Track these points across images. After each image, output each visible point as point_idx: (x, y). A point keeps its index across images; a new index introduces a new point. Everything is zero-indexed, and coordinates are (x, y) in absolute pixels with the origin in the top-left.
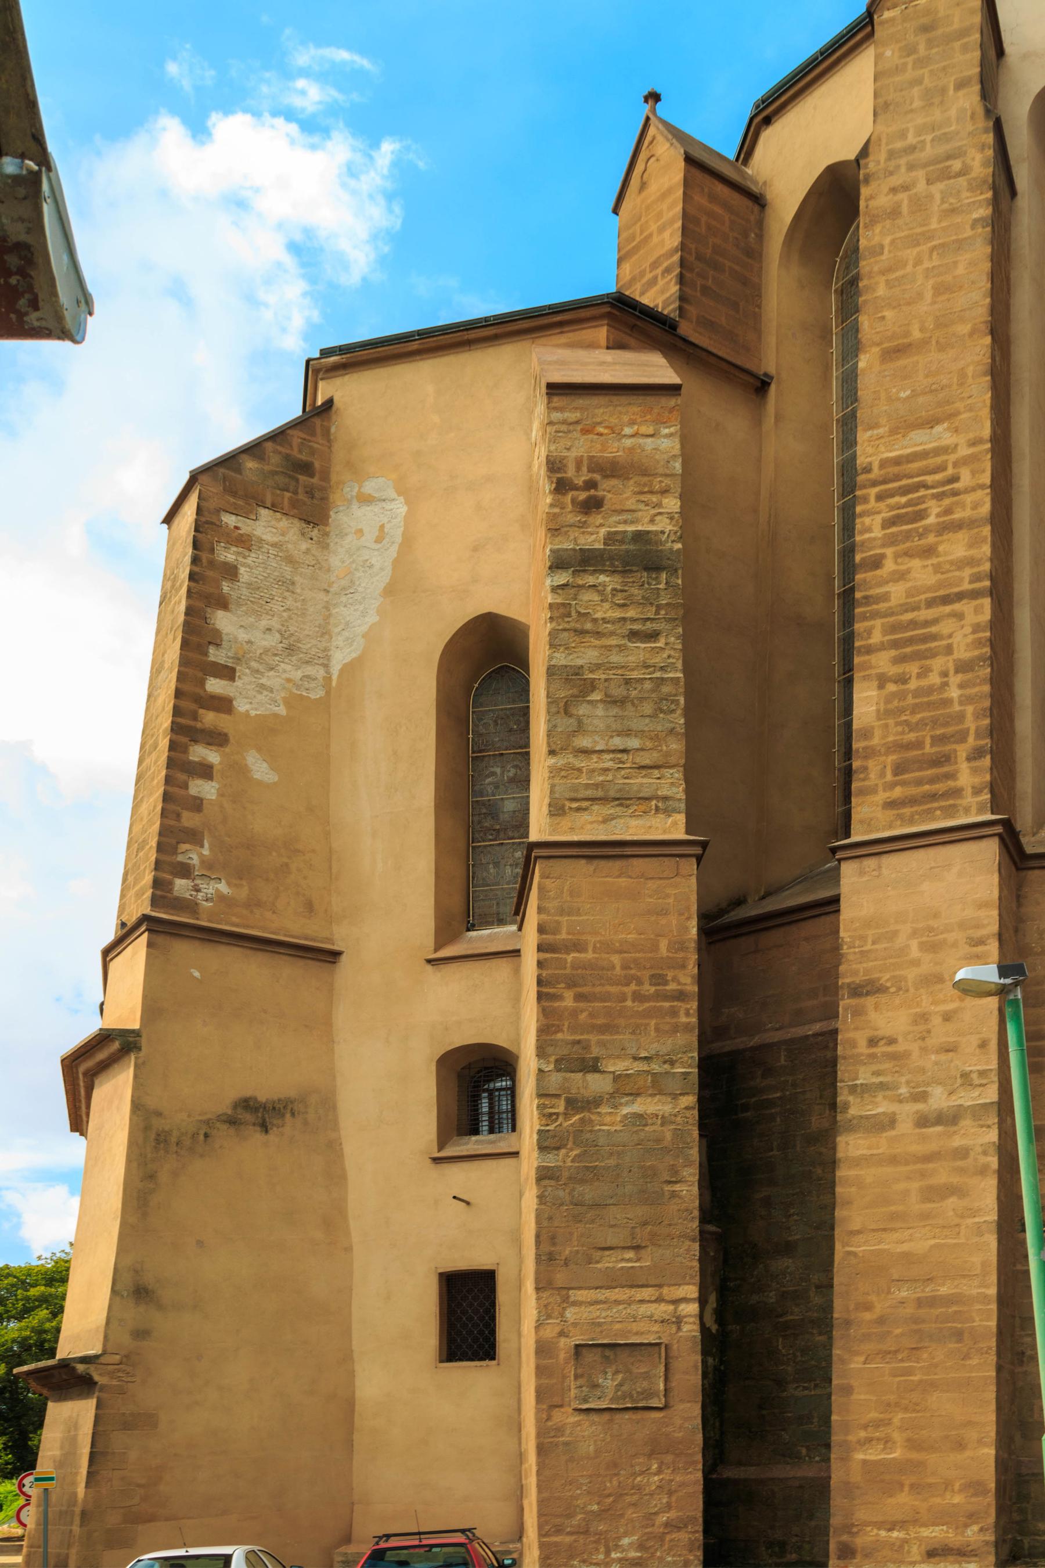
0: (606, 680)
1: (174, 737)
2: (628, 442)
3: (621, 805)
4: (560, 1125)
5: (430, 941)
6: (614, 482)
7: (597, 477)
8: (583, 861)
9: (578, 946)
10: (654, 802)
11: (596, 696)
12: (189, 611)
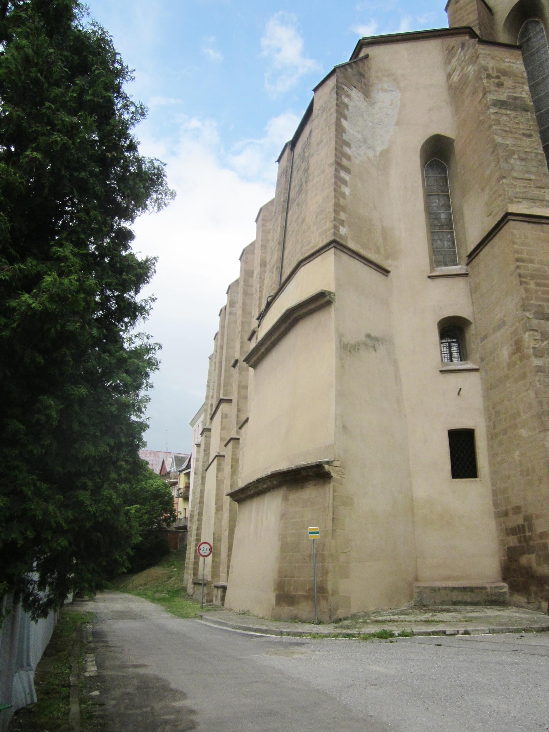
0: (518, 151)
1: (337, 166)
2: (507, 64)
3: (533, 202)
4: (540, 345)
5: (427, 267)
6: (505, 77)
7: (500, 75)
8: (526, 224)
9: (531, 261)
10: (545, 202)
11: (516, 156)
12: (337, 118)
